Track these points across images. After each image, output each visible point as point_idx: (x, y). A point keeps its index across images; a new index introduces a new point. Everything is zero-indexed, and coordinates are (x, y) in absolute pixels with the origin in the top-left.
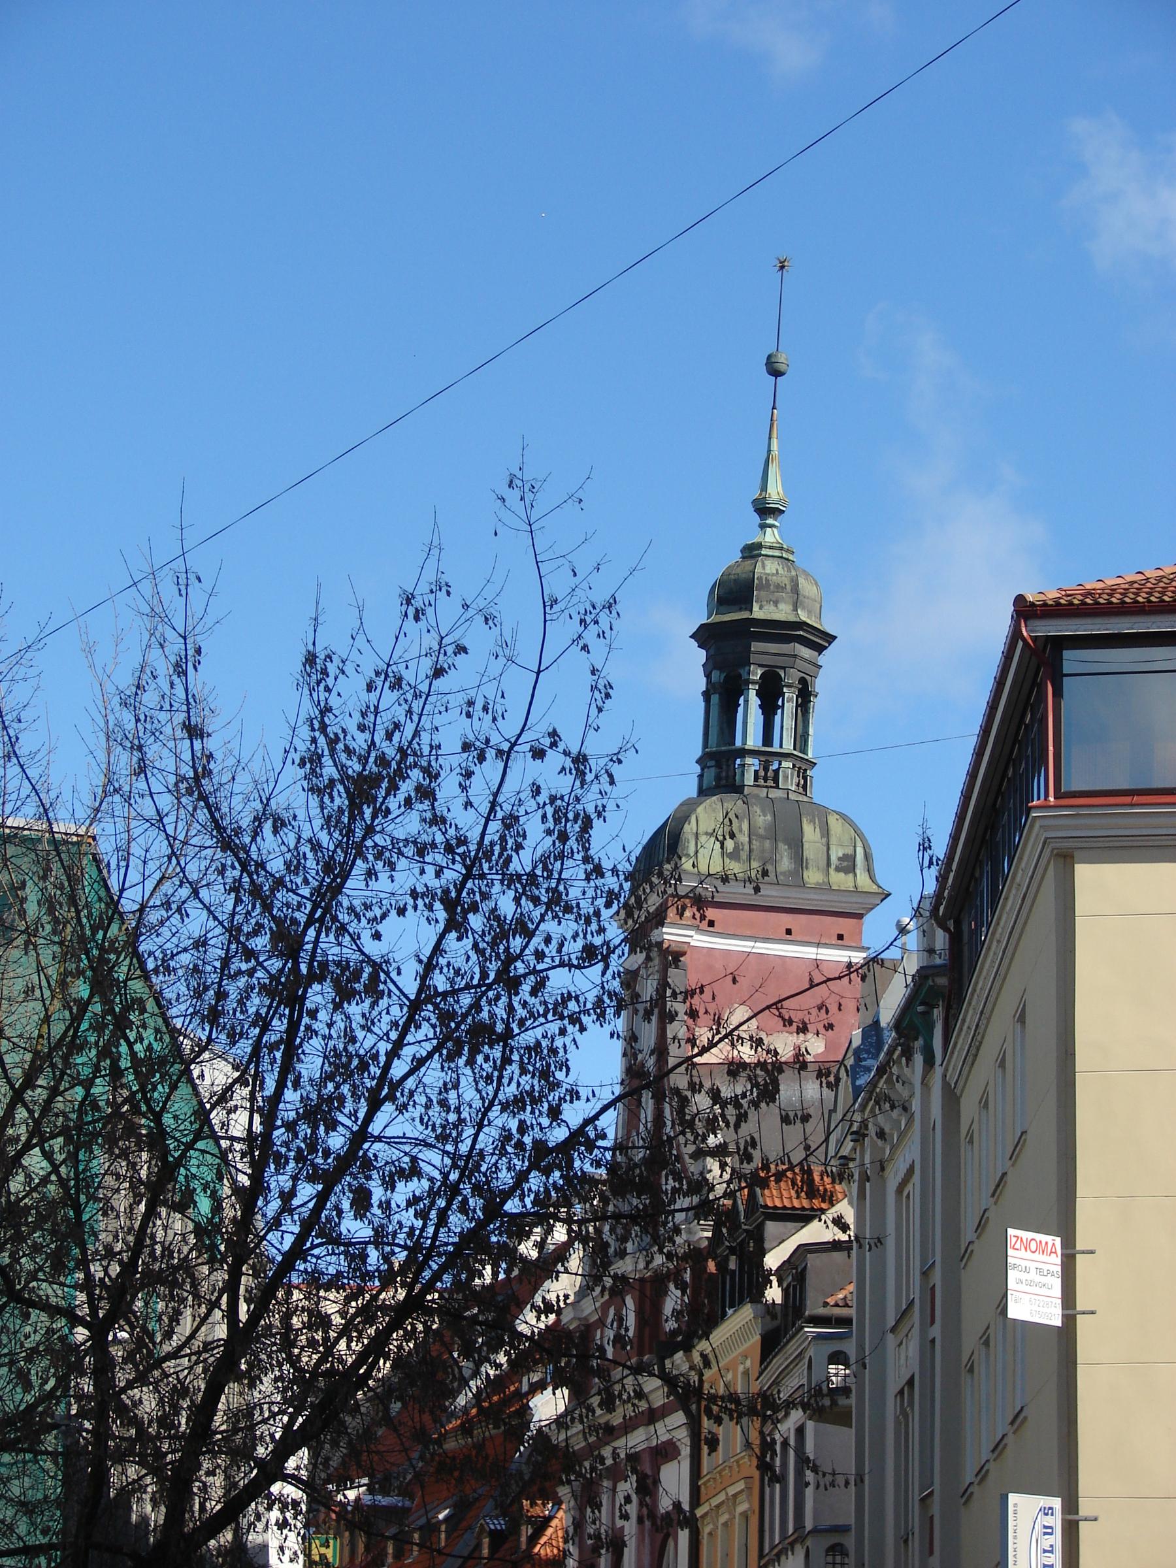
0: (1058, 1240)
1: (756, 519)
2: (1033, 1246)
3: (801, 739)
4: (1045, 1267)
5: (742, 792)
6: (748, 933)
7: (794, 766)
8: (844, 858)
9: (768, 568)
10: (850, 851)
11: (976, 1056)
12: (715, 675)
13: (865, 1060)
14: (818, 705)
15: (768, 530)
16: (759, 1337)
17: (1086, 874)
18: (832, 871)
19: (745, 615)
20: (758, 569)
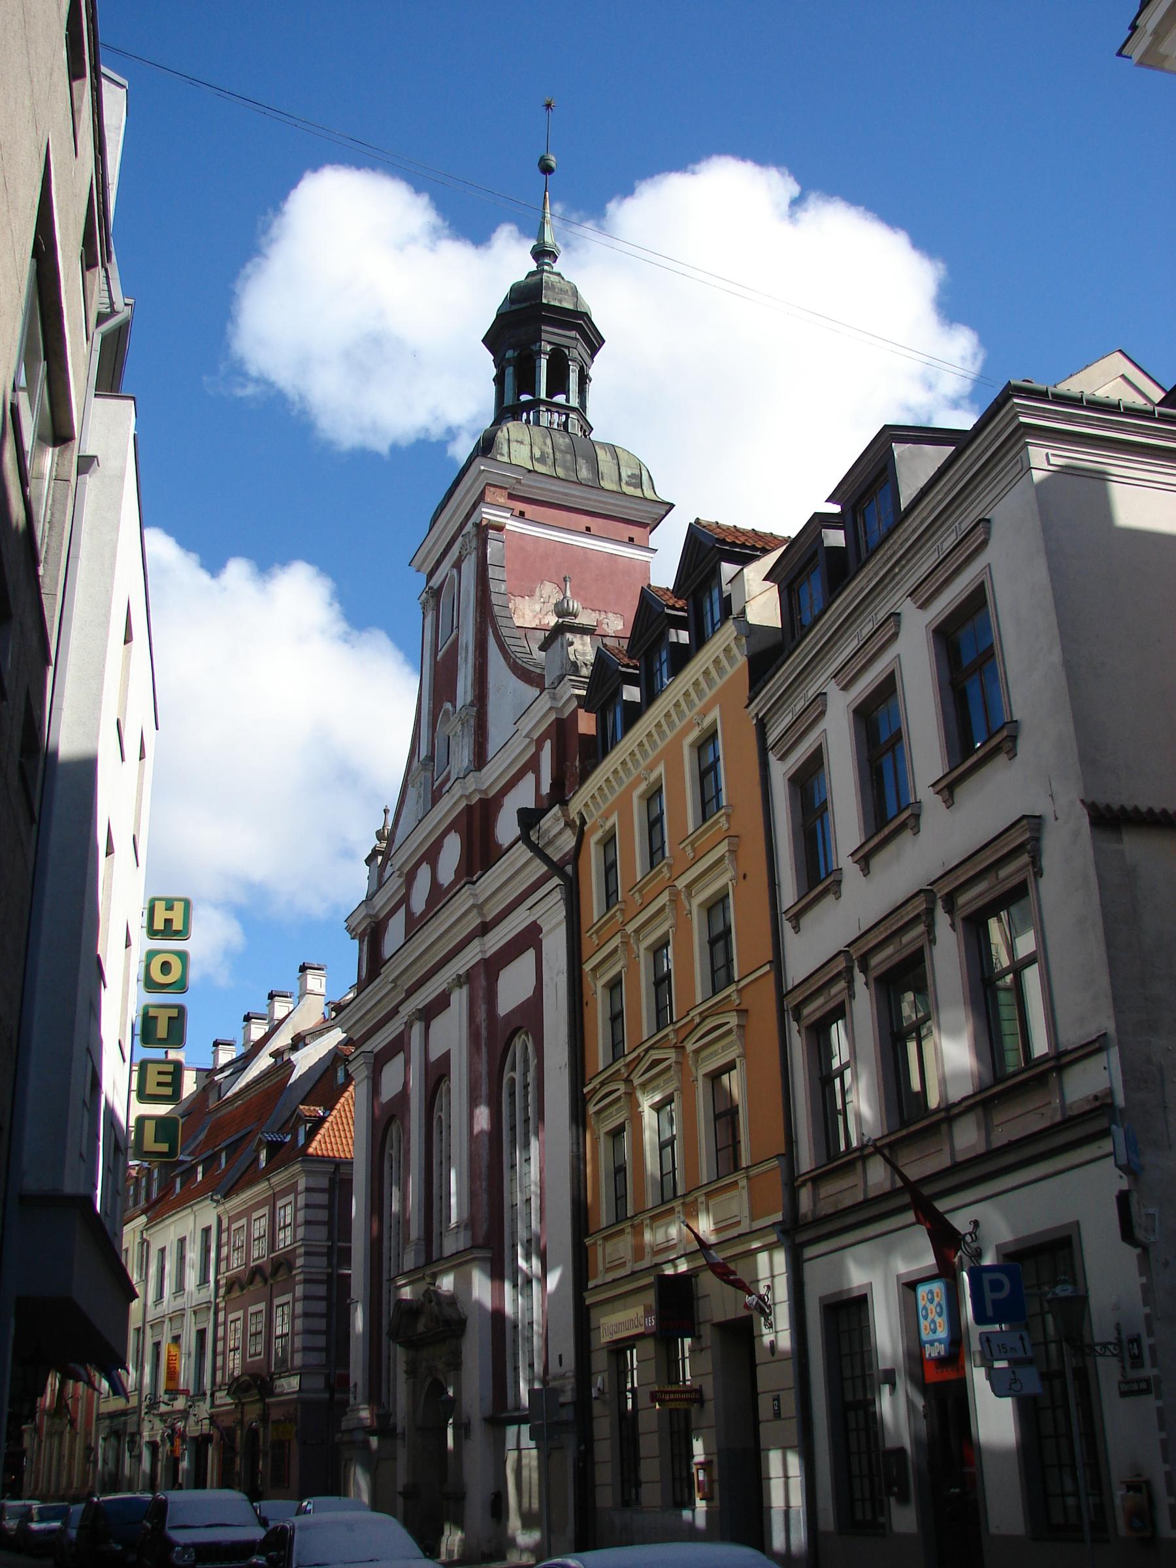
8: (632, 476)
10: (637, 472)
16: (745, 659)
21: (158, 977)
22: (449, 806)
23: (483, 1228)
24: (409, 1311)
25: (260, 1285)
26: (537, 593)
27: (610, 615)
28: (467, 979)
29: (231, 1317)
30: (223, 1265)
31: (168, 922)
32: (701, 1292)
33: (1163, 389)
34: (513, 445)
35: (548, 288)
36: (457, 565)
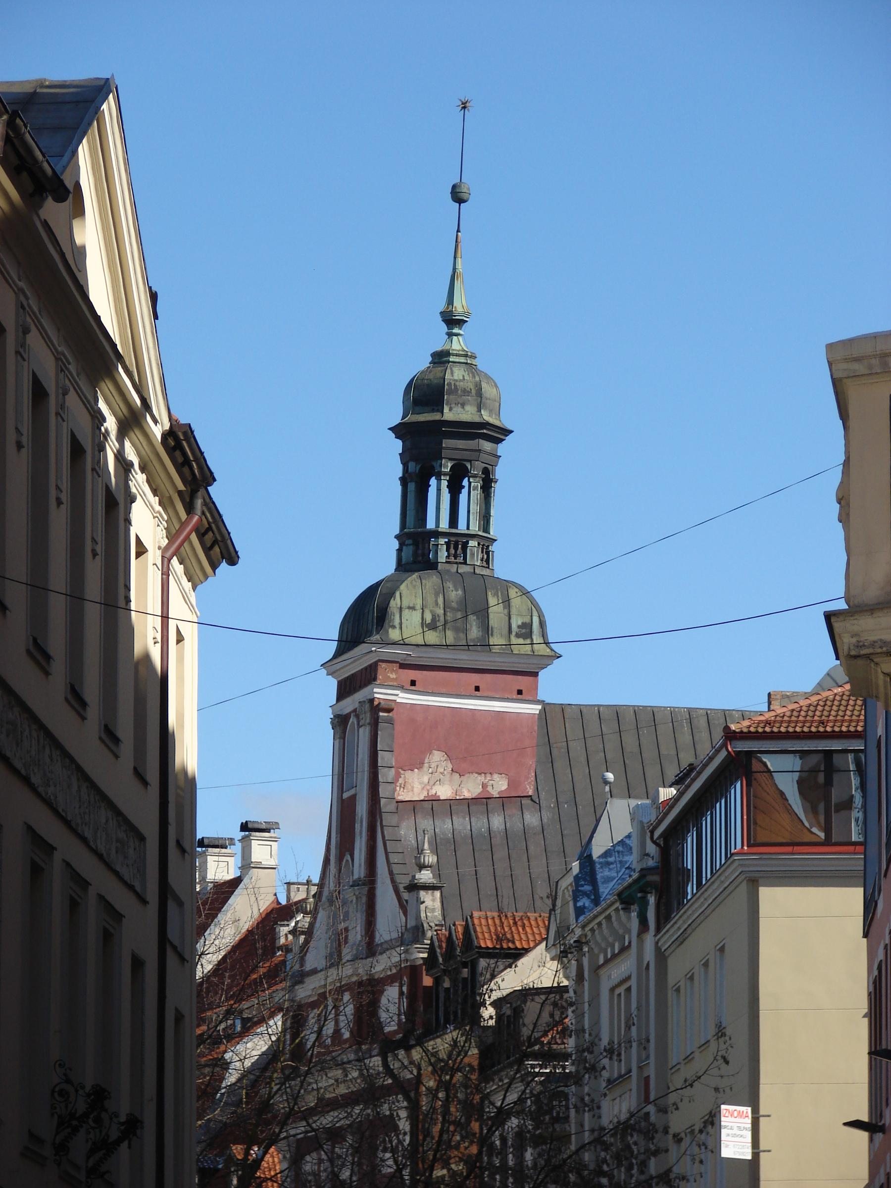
0: (749, 1109)
1: (444, 328)
2: (736, 1114)
3: (485, 519)
4: (742, 1125)
5: (436, 568)
6: (444, 691)
7: (479, 544)
8: (524, 626)
9: (456, 374)
11: (682, 943)
12: (412, 466)
13: (582, 886)
14: (498, 490)
15: (455, 338)
17: (768, 895)
18: (513, 637)
19: (436, 416)
20: (448, 376)
26: (426, 765)
27: (496, 776)
32: (866, 1020)
33: (764, 1116)
34: (406, 613)
35: (450, 392)
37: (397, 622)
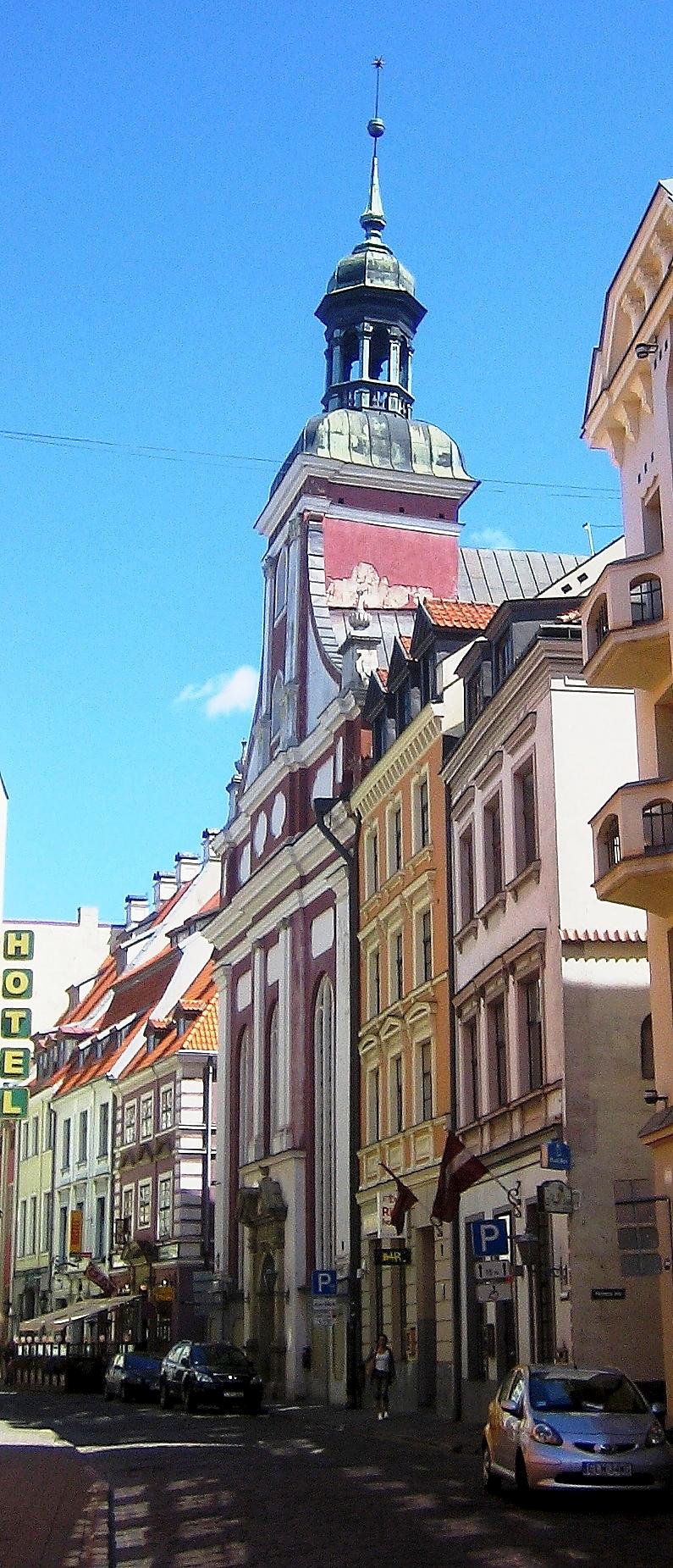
21: (11, 989)
22: (276, 772)
23: (299, 1132)
24: (253, 1196)
25: (147, 1161)
28: (289, 922)
29: (126, 1188)
30: (117, 1212)
31: (18, 949)
36: (288, 543)
37: (325, 444)
